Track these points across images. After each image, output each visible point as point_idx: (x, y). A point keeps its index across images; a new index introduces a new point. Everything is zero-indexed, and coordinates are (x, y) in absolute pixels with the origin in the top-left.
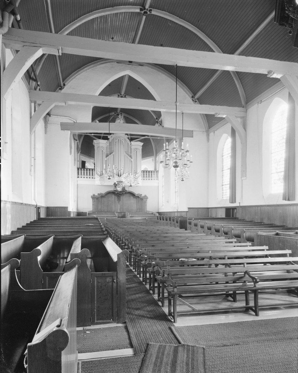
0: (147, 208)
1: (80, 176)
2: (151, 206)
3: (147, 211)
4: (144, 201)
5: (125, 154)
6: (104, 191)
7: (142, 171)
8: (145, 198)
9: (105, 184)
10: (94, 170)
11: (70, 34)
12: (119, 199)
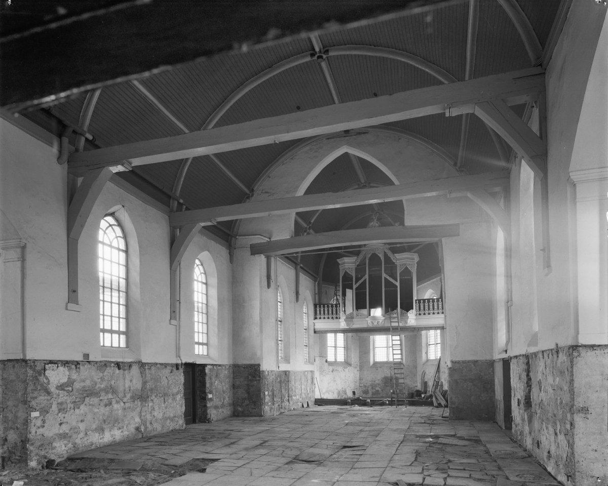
1: (318, 316)
11: (218, 125)
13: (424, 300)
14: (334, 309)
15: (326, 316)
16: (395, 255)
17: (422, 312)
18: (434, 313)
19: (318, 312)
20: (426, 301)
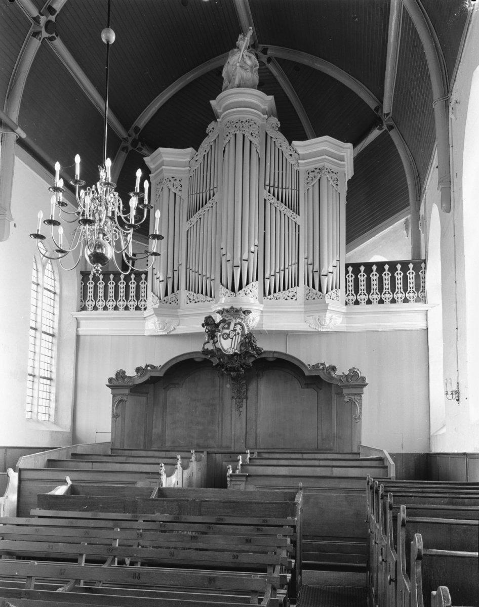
0: (360, 438)
1: (90, 303)
2: (383, 428)
3: (360, 446)
4: (346, 399)
5: (265, 194)
6: (160, 357)
7: (347, 266)
8: (351, 382)
9: (180, 330)
10: (143, 276)
12: (241, 396)
13: (368, 266)
14: (132, 286)
15: (121, 304)
16: (295, 143)
17: (363, 297)
18: (393, 301)
19: (90, 293)
20: (374, 268)
